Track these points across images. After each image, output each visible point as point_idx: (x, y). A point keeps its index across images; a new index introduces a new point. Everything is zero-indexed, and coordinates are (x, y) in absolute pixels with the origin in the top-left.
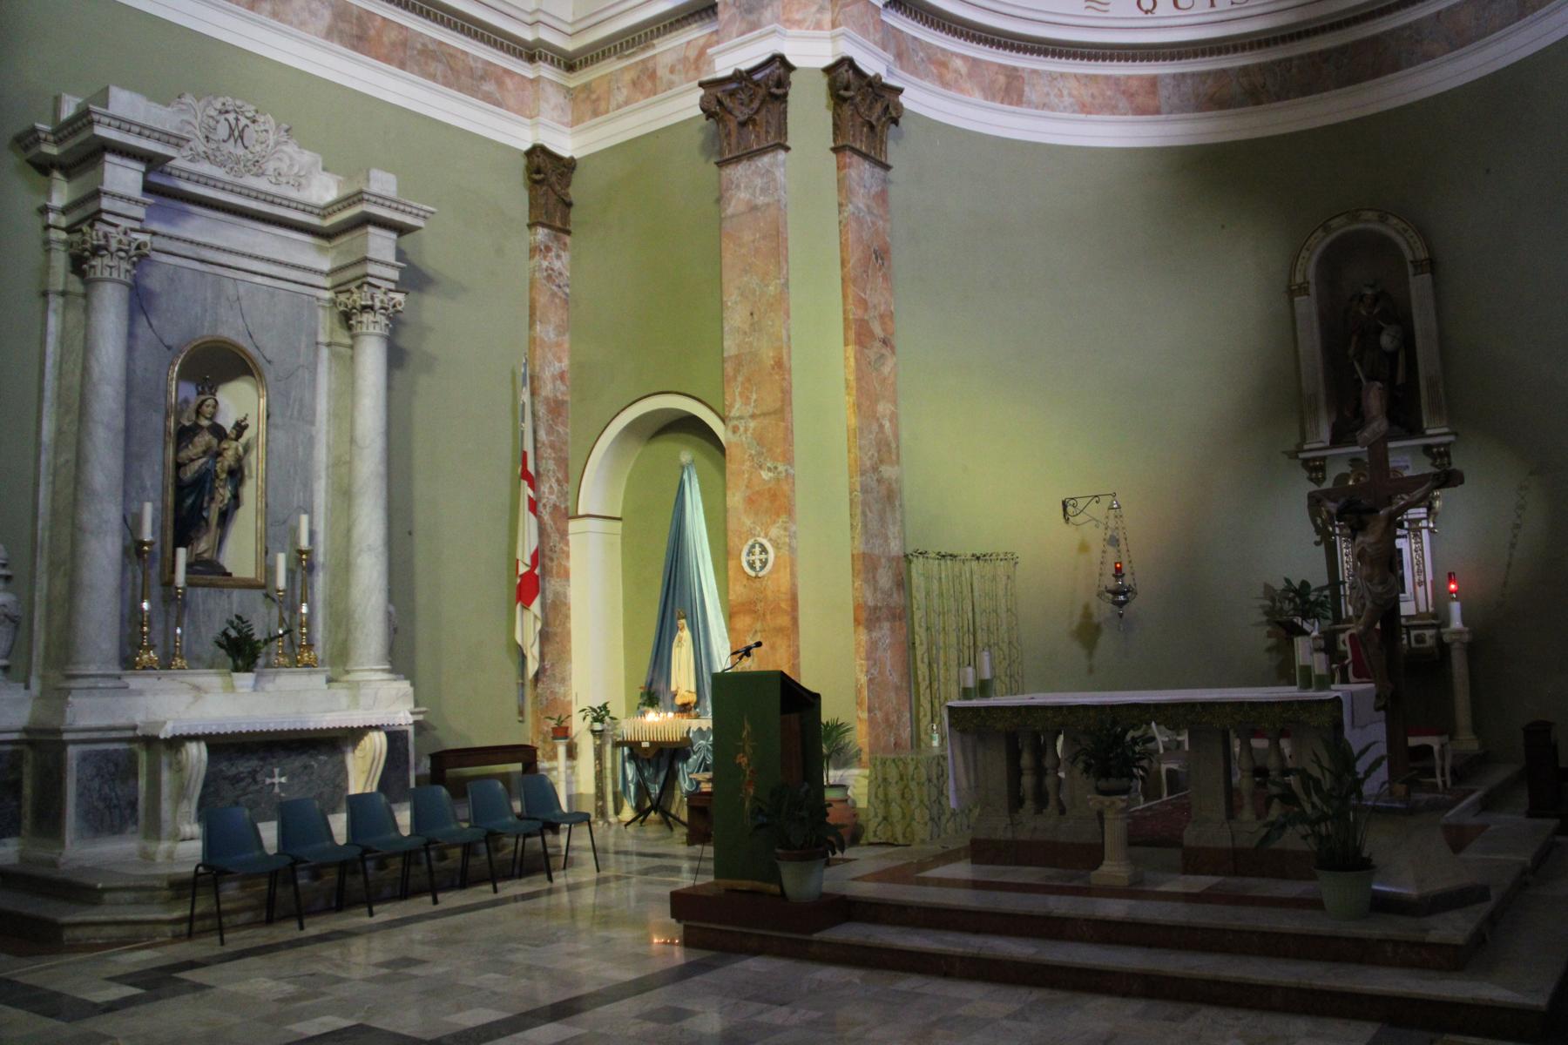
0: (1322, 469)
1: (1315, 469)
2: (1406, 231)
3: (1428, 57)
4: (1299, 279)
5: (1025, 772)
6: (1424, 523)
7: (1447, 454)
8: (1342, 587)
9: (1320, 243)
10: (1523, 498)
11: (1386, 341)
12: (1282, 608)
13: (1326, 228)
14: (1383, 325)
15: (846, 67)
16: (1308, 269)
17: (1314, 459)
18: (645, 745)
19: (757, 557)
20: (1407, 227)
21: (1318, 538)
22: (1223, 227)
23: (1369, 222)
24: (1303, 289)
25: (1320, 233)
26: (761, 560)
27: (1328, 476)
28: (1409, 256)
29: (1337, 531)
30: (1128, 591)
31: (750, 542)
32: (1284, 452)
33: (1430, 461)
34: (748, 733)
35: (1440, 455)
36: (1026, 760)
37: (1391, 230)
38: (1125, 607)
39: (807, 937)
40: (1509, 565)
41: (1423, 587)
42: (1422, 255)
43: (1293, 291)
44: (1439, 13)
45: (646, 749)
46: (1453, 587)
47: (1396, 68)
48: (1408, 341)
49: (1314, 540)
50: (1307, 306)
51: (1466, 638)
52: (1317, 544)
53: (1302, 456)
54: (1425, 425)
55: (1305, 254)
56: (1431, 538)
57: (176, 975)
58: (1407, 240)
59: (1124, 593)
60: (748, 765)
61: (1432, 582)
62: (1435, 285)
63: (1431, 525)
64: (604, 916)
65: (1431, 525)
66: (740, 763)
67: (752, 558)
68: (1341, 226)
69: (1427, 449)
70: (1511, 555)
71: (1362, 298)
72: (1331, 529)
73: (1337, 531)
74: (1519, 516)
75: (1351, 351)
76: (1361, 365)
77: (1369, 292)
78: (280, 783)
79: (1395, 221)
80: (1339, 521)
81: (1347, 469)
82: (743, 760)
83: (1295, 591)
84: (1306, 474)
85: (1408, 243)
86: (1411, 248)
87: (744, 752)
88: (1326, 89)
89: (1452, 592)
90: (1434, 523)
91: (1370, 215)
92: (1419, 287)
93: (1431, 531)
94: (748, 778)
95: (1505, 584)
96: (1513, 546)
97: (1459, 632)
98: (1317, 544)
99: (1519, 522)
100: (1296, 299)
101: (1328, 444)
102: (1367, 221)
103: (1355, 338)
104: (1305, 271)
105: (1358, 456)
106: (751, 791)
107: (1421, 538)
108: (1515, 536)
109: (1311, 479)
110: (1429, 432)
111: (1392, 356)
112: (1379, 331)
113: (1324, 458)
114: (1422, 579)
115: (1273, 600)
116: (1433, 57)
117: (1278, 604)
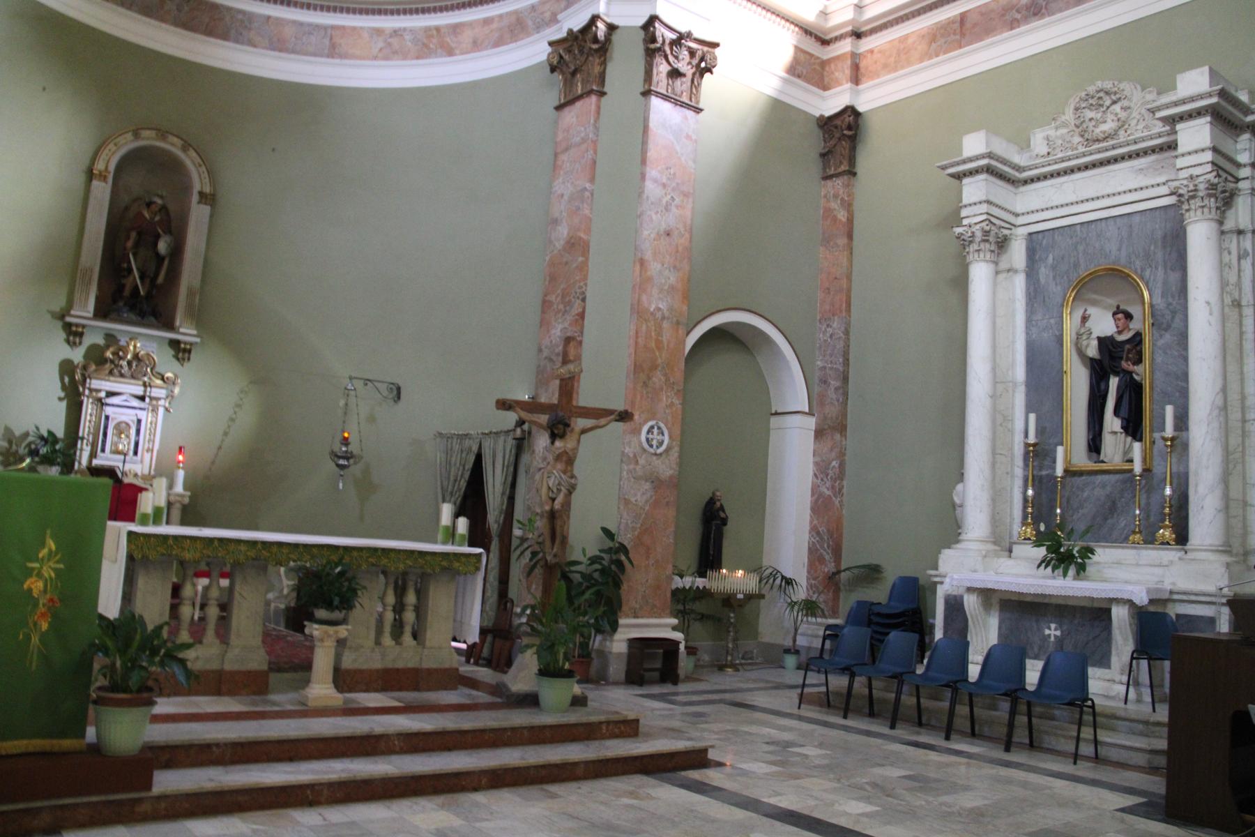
0: (81, 335)
1: (73, 334)
2: (200, 166)
3: (252, 44)
4: (100, 166)
5: (391, 608)
6: (162, 402)
7: (189, 351)
8: (79, 442)
9: (127, 144)
10: (241, 399)
11: (162, 247)
12: (17, 452)
13: (136, 135)
14: (161, 233)
15: (849, 113)
16: (109, 160)
17: (77, 325)
18: (740, 596)
19: (655, 435)
20: (202, 163)
21: (62, 394)
22: (44, 89)
23: (172, 146)
24: (103, 177)
25: (129, 136)
26: (652, 434)
27: (83, 344)
28: (197, 187)
29: (87, 392)
30: (352, 457)
31: (650, 423)
32: (48, 311)
33: (172, 352)
34: (50, 550)
35: (185, 351)
36: (411, 598)
37: (189, 160)
38: (346, 470)
39: (143, 794)
40: (220, 448)
41: (150, 454)
42: (207, 190)
43: (90, 175)
44: (269, 18)
45: (740, 600)
46: (181, 458)
47: (225, 36)
48: (177, 251)
49: (57, 395)
50: (102, 191)
51: (186, 500)
52: (60, 399)
53: (68, 319)
54: (178, 323)
55: (111, 146)
56: (164, 415)
57: (1145, 800)
58: (113, 154)
59: (347, 459)
60: (45, 591)
61: (158, 451)
62: (212, 216)
63: (167, 405)
64: (823, 735)
65: (167, 405)
66: (30, 590)
67: (650, 436)
68: (149, 139)
69: (174, 344)
70: (223, 441)
71: (149, 205)
72: (81, 389)
73: (87, 392)
74: (235, 413)
75: (130, 244)
76: (134, 255)
77: (159, 201)
78: (1055, 635)
79: (194, 154)
80: (1165, 520)
81: (100, 341)
82: (36, 585)
83: (42, 438)
84: (63, 335)
85: (200, 176)
86: (199, 182)
87: (40, 575)
88: (163, 20)
89: (179, 462)
90: (170, 403)
91: (175, 140)
92: (198, 215)
93: (167, 410)
94: (42, 609)
95: (213, 463)
96: (226, 434)
97: (182, 496)
98: (60, 399)
99: (234, 416)
100: (95, 183)
101: (91, 315)
102: (173, 144)
103: (133, 235)
104: (108, 161)
105: (115, 333)
106: (45, 626)
107: (157, 414)
108: (229, 427)
109: (68, 342)
110: (182, 330)
111: (160, 259)
112: (158, 237)
113: (84, 326)
114: (151, 447)
115: (10, 442)
116: (255, 46)
117: (14, 447)
